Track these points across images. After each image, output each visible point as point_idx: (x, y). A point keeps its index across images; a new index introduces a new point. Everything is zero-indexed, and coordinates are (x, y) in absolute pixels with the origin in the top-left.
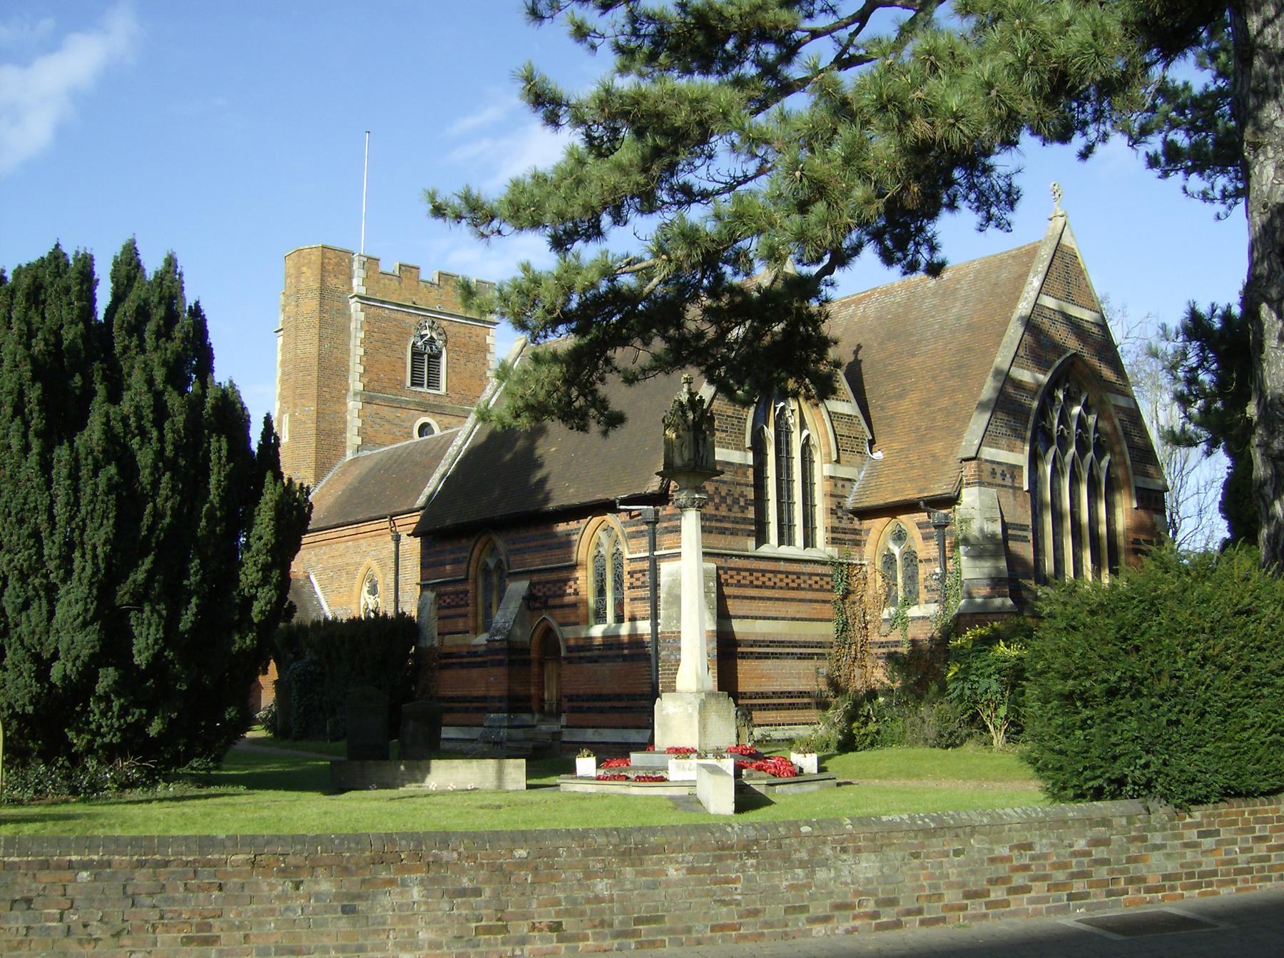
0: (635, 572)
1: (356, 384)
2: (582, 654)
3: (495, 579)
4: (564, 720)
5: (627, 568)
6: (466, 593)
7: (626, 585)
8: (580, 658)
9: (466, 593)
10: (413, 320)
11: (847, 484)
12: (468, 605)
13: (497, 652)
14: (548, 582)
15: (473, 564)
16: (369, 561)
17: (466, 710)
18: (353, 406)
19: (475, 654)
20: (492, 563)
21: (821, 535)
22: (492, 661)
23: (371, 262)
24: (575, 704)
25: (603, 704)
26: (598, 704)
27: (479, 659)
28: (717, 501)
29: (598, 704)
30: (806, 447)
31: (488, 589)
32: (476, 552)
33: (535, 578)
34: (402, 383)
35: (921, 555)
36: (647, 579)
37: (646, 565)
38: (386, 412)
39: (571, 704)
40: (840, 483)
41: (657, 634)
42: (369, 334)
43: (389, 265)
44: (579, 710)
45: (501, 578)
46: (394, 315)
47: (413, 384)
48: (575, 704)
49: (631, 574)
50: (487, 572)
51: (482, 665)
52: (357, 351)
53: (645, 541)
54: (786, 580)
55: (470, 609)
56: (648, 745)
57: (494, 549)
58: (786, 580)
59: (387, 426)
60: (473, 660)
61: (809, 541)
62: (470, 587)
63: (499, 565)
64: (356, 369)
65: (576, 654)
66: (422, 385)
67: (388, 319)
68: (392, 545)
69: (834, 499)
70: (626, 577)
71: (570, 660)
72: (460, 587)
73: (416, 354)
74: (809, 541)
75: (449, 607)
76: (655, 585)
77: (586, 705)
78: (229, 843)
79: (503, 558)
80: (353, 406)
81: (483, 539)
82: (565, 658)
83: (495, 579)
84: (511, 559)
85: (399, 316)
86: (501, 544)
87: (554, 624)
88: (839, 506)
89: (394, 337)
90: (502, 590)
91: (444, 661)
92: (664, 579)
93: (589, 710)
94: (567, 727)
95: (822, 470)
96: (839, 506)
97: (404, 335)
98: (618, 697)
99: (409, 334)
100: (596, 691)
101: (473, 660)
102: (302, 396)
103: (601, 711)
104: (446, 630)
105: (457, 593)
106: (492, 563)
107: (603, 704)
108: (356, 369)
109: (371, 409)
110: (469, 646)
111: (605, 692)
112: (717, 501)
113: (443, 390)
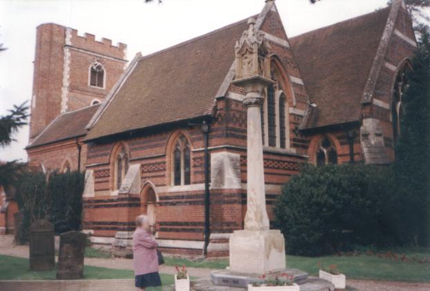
0: (197, 158)
1: (66, 83)
2: (167, 201)
3: (123, 163)
4: (157, 235)
5: (192, 156)
6: (109, 170)
7: (192, 165)
8: (166, 203)
9: (109, 170)
10: (90, 58)
11: (300, 118)
12: (109, 176)
13: (122, 199)
14: (150, 164)
15: (112, 156)
16: (67, 158)
17: (107, 229)
18: (65, 91)
19: (112, 201)
20: (122, 155)
21: (288, 142)
22: (120, 204)
23: (74, 32)
24: (163, 227)
25: (178, 227)
26: (175, 227)
27: (114, 203)
28: (241, 121)
29: (175, 227)
30: (282, 99)
31: (120, 168)
32: (114, 150)
33: (144, 162)
34: (86, 84)
35: (339, 152)
36: (203, 162)
37: (202, 155)
38: (79, 96)
39: (161, 227)
40: (297, 117)
41: (208, 191)
42: (72, 62)
43: (81, 33)
44: (165, 230)
45: (126, 163)
46: (83, 55)
47: (91, 84)
48: (163, 227)
49: (194, 159)
50: (120, 160)
51: (116, 206)
52: (67, 69)
53: (202, 143)
54: (273, 164)
55: (110, 178)
56: (228, 265)
57: (124, 148)
58: (273, 164)
59: (79, 102)
60: (111, 203)
61: (283, 145)
62: (110, 167)
63: (125, 157)
64: (66, 76)
65: (165, 201)
66: (95, 85)
67: (80, 57)
68: (77, 151)
69: (294, 125)
70: (192, 161)
71: (161, 204)
72: (106, 168)
73: (93, 72)
74: (283, 145)
75: (100, 177)
76: (208, 165)
77: (169, 227)
78: (243, 168)
79: (128, 152)
80: (65, 91)
81: (118, 143)
82: (158, 203)
83: (123, 163)
84: (132, 153)
85: (84, 55)
86: (127, 145)
87: (153, 186)
88: (296, 128)
89: (83, 64)
90: (127, 168)
91: (97, 204)
92: (213, 163)
93: (171, 230)
94: (159, 239)
95: (289, 110)
96: (296, 128)
97: (87, 63)
98: (187, 224)
99: (90, 63)
100: (175, 220)
101: (111, 203)
102: (42, 87)
103: (177, 231)
104: (98, 188)
105: (104, 171)
106: (122, 155)
107: (178, 227)
108: (66, 76)
109: (72, 94)
110: (109, 196)
111: (179, 220)
112: (241, 121)
113: (104, 88)
